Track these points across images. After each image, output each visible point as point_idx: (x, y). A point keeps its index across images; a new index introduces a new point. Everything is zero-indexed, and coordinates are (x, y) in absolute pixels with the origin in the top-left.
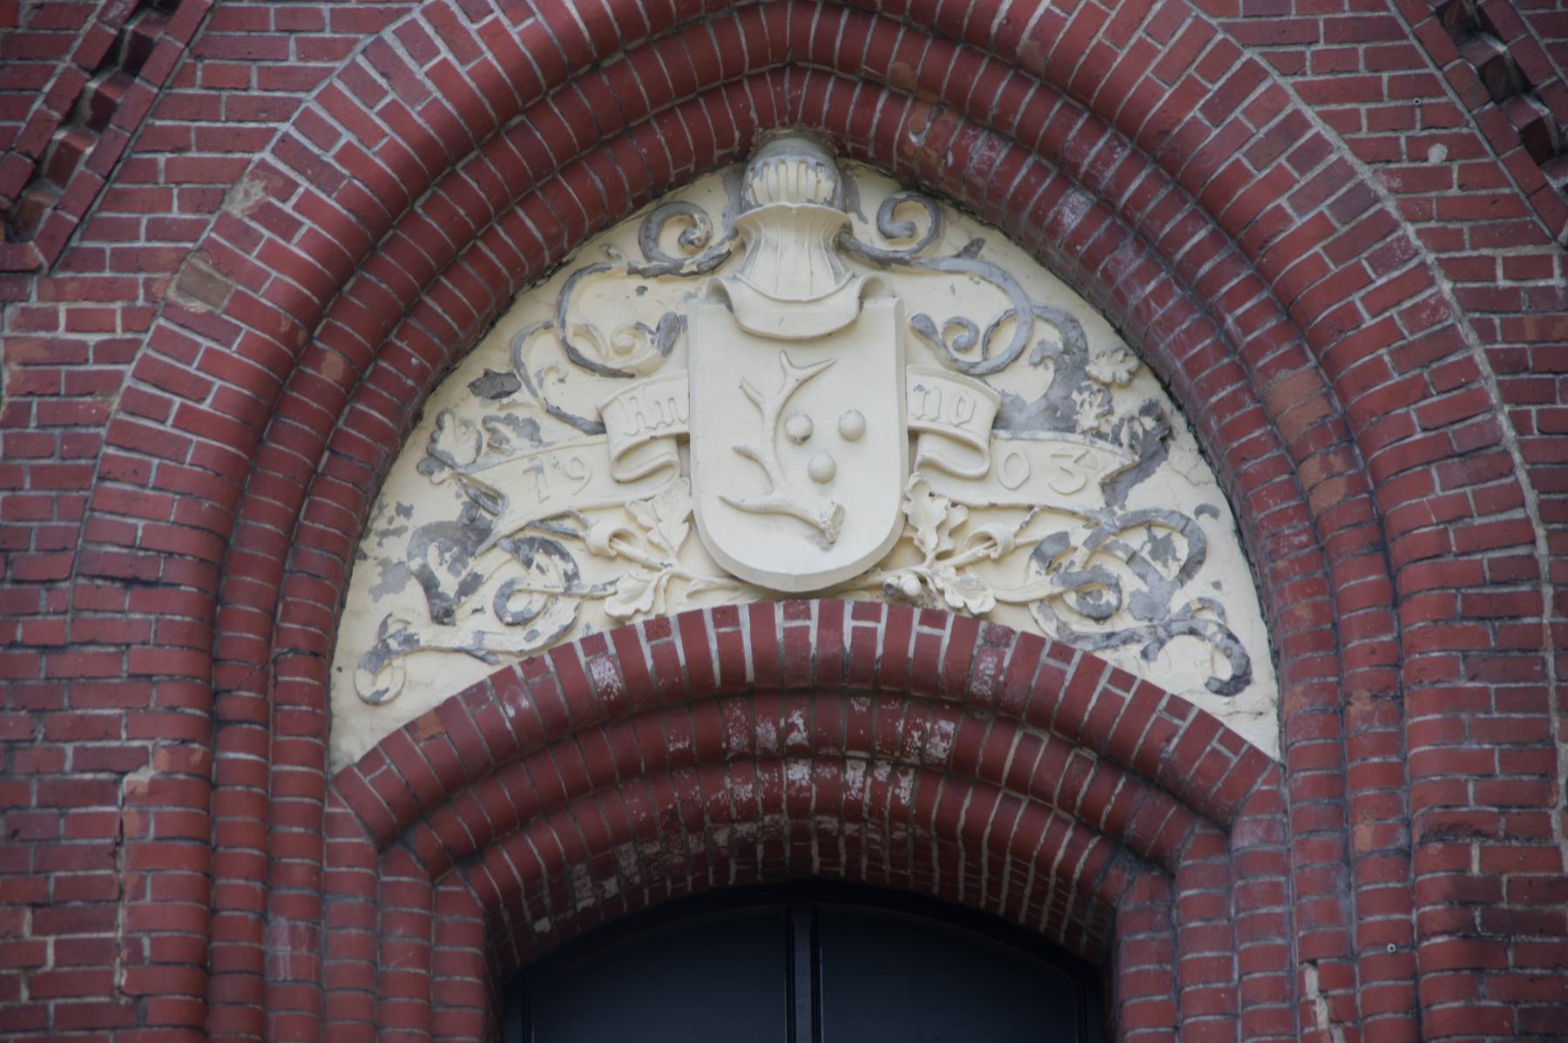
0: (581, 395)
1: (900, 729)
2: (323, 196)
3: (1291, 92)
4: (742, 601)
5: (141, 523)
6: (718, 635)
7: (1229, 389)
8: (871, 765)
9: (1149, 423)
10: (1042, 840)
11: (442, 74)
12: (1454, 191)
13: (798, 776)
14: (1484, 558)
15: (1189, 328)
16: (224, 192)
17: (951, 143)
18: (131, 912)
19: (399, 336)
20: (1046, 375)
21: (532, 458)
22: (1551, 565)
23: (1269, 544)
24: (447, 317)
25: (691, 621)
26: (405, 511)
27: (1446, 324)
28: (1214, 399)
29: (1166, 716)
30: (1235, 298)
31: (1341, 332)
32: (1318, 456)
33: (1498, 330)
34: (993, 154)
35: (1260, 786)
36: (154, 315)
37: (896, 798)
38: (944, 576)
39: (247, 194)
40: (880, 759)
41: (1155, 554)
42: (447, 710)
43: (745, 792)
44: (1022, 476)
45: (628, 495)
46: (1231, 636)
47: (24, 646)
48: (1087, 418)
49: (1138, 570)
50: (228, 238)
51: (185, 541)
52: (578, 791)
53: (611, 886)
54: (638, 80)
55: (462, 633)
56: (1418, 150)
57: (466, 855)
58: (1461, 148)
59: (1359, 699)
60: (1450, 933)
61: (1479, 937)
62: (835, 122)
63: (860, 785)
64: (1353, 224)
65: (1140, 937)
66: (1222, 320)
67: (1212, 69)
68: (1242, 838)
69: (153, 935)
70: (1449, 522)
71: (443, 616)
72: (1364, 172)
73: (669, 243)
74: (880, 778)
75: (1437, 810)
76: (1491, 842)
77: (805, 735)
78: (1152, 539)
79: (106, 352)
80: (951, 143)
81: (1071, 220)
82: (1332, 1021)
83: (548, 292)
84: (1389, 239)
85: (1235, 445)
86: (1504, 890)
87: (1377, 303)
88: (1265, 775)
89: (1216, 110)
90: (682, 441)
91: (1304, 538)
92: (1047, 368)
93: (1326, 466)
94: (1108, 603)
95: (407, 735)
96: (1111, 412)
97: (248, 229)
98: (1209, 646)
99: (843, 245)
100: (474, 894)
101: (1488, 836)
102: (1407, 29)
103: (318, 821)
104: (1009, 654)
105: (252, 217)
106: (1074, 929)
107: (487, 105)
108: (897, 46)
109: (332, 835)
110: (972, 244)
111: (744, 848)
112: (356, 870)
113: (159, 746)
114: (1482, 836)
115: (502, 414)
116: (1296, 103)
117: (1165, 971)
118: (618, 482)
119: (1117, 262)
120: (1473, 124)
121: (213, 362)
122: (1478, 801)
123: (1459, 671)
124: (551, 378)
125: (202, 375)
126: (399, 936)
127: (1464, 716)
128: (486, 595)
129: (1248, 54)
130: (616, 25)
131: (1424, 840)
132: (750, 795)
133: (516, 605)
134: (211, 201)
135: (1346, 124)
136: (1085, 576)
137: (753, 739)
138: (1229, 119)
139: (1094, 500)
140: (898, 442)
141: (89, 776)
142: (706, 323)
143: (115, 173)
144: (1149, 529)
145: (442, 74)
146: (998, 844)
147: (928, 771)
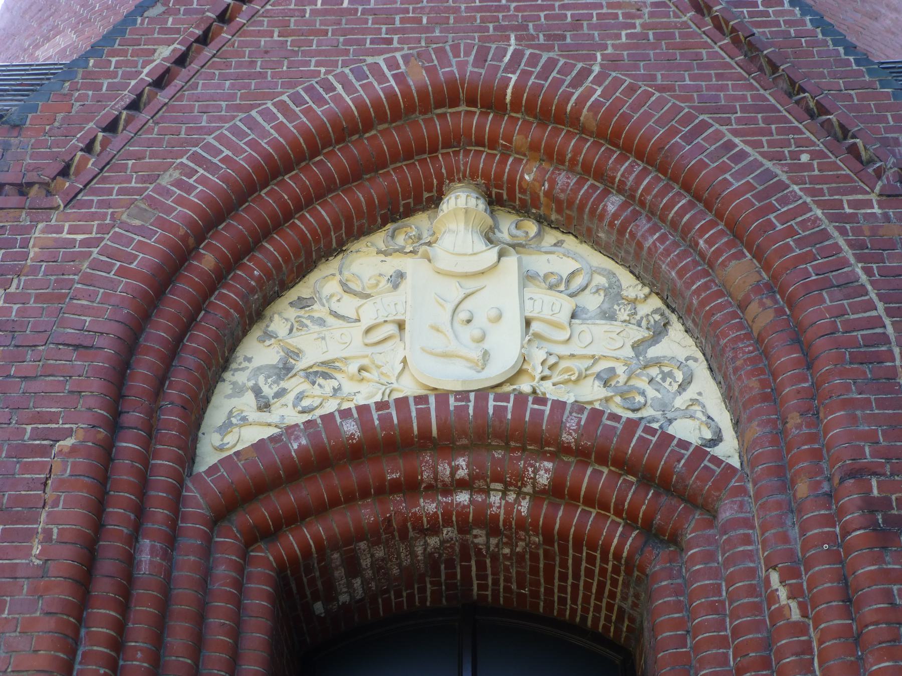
0: (348, 305)
1: (522, 466)
2: (210, 176)
3: (726, 132)
5: (88, 319)
6: (417, 409)
7: (703, 281)
8: (504, 494)
9: (657, 317)
10: (604, 534)
11: (280, 128)
12: (816, 172)
13: (462, 499)
15: (678, 253)
16: (159, 175)
17: (546, 178)
18: (49, 514)
19: (249, 260)
20: (599, 299)
21: (319, 333)
22: (896, 338)
23: (731, 354)
24: (275, 253)
25: (402, 403)
26: (249, 360)
27: (821, 228)
28: (694, 287)
29: (677, 449)
30: (703, 230)
31: (765, 232)
32: (757, 301)
33: (849, 231)
34: (569, 181)
35: (733, 483)
36: (113, 226)
37: (519, 512)
39: (171, 175)
40: (510, 491)
41: (664, 380)
44: (589, 340)
45: (369, 351)
46: (709, 417)
47: (14, 377)
48: (623, 315)
49: (656, 387)
50: (158, 194)
51: (114, 329)
52: (334, 502)
54: (383, 143)
55: (274, 416)
56: (795, 156)
58: (815, 155)
59: (792, 418)
60: (865, 528)
61: (882, 530)
62: (486, 175)
63: (498, 505)
64: (766, 185)
65: (664, 583)
66: (697, 244)
68: (725, 513)
69: (60, 527)
70: (837, 317)
71: (265, 406)
72: (768, 164)
73: (401, 240)
74: (510, 501)
75: (848, 462)
76: (883, 478)
77: (466, 471)
78: (662, 372)
79: (84, 243)
80: (546, 178)
81: (611, 208)
82: (789, 598)
84: (785, 192)
85: (708, 308)
86: (894, 504)
87: (783, 218)
88: (736, 478)
90: (401, 326)
91: (751, 348)
92: (599, 295)
93: (762, 304)
94: (639, 402)
95: (235, 458)
96: (635, 313)
97: (168, 190)
98: (698, 422)
99: (489, 238)
100: (271, 558)
101: (881, 475)
102: (782, 109)
104: (584, 417)
105: (172, 185)
107: (302, 141)
108: (518, 127)
109: (184, 507)
110: (558, 243)
112: (198, 526)
113: (80, 427)
114: (877, 475)
115: (307, 315)
116: (729, 136)
117: (680, 601)
118: (366, 345)
119: (637, 226)
120: (821, 145)
121: (141, 246)
122: (872, 456)
123: (852, 389)
124: (335, 299)
125: (134, 252)
127: (858, 413)
128: (290, 398)
129: (701, 117)
130: (371, 110)
131: (842, 480)
132: (435, 510)
133: (305, 403)
135: (756, 145)
136: (625, 388)
137: (436, 473)
138: (695, 142)
139: (629, 352)
140: (517, 325)
141: (38, 442)
143: (106, 169)
144: (660, 367)
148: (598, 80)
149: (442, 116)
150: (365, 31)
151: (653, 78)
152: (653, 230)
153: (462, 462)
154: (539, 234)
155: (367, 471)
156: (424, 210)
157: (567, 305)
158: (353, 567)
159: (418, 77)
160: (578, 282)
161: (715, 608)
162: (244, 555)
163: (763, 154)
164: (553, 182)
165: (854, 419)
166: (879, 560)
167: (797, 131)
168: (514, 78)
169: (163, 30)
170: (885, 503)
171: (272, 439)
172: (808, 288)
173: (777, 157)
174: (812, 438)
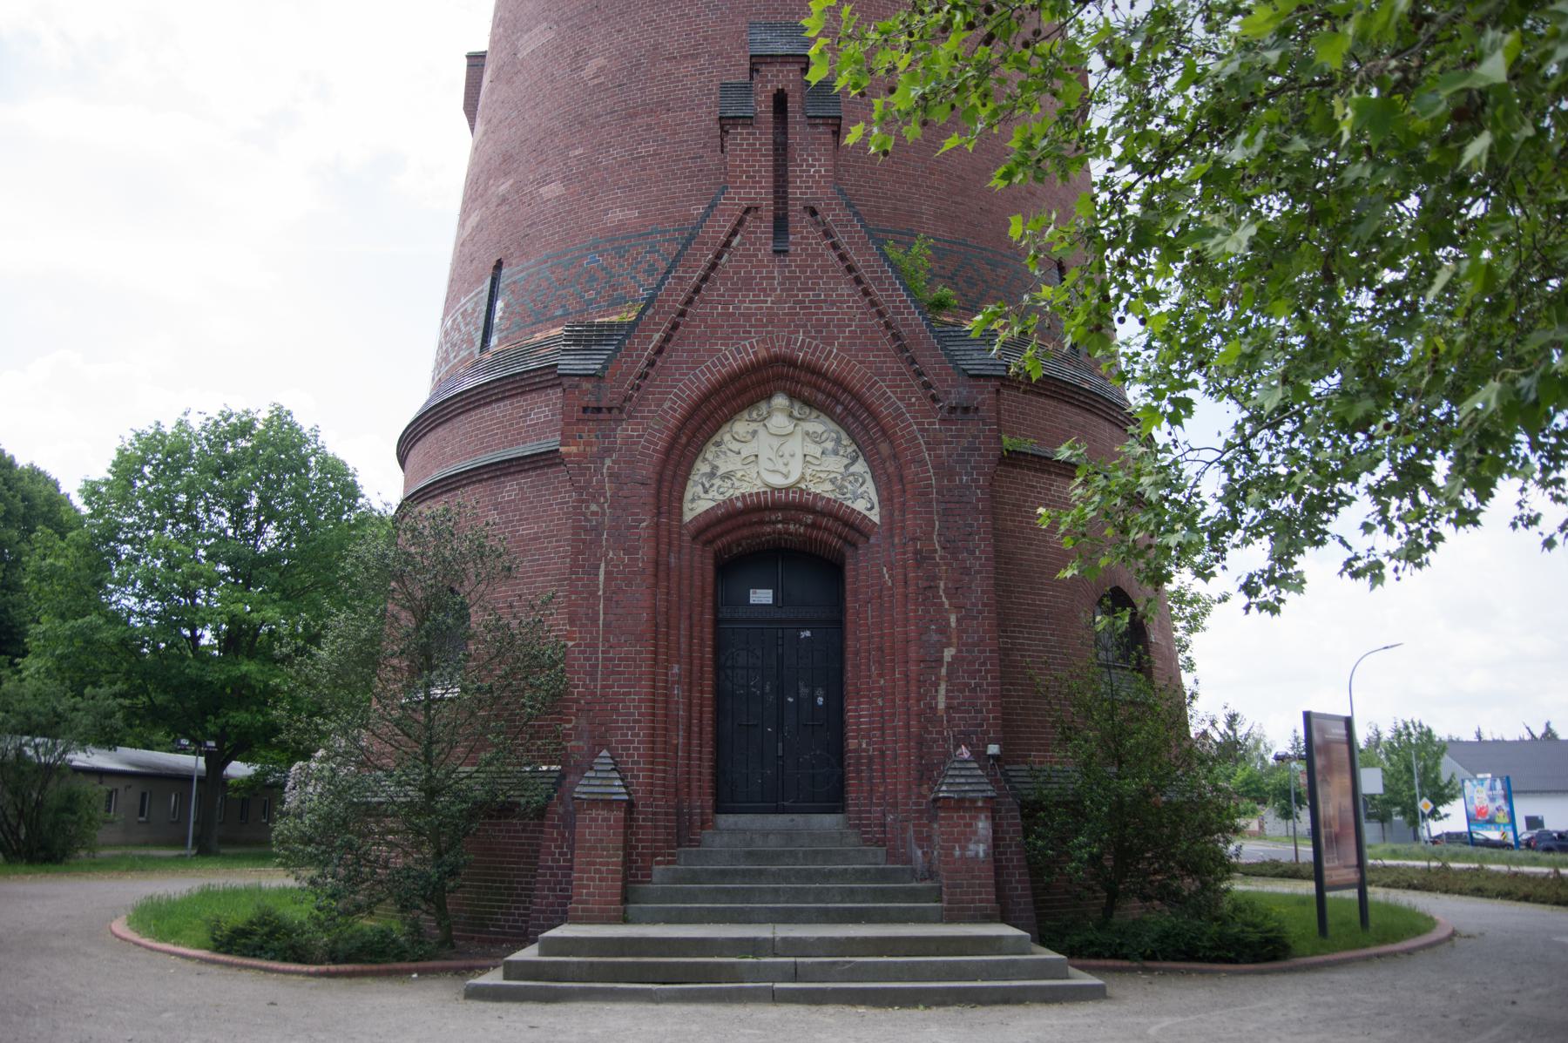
0: (735, 446)
11: (708, 379)
48: (841, 453)
55: (710, 496)
58: (918, 399)
67: (868, 381)
71: (706, 492)
79: (638, 436)
83: (729, 424)
87: (901, 430)
99: (791, 416)
103: (680, 534)
111: (768, 541)
121: (660, 439)
128: (715, 488)
139: (842, 470)
142: (762, 433)
145: (708, 379)
147: (807, 526)
148: (835, 358)
150: (740, 326)
158: (740, 545)
159: (763, 354)
169: (655, 324)
171: (712, 508)
173: (901, 399)
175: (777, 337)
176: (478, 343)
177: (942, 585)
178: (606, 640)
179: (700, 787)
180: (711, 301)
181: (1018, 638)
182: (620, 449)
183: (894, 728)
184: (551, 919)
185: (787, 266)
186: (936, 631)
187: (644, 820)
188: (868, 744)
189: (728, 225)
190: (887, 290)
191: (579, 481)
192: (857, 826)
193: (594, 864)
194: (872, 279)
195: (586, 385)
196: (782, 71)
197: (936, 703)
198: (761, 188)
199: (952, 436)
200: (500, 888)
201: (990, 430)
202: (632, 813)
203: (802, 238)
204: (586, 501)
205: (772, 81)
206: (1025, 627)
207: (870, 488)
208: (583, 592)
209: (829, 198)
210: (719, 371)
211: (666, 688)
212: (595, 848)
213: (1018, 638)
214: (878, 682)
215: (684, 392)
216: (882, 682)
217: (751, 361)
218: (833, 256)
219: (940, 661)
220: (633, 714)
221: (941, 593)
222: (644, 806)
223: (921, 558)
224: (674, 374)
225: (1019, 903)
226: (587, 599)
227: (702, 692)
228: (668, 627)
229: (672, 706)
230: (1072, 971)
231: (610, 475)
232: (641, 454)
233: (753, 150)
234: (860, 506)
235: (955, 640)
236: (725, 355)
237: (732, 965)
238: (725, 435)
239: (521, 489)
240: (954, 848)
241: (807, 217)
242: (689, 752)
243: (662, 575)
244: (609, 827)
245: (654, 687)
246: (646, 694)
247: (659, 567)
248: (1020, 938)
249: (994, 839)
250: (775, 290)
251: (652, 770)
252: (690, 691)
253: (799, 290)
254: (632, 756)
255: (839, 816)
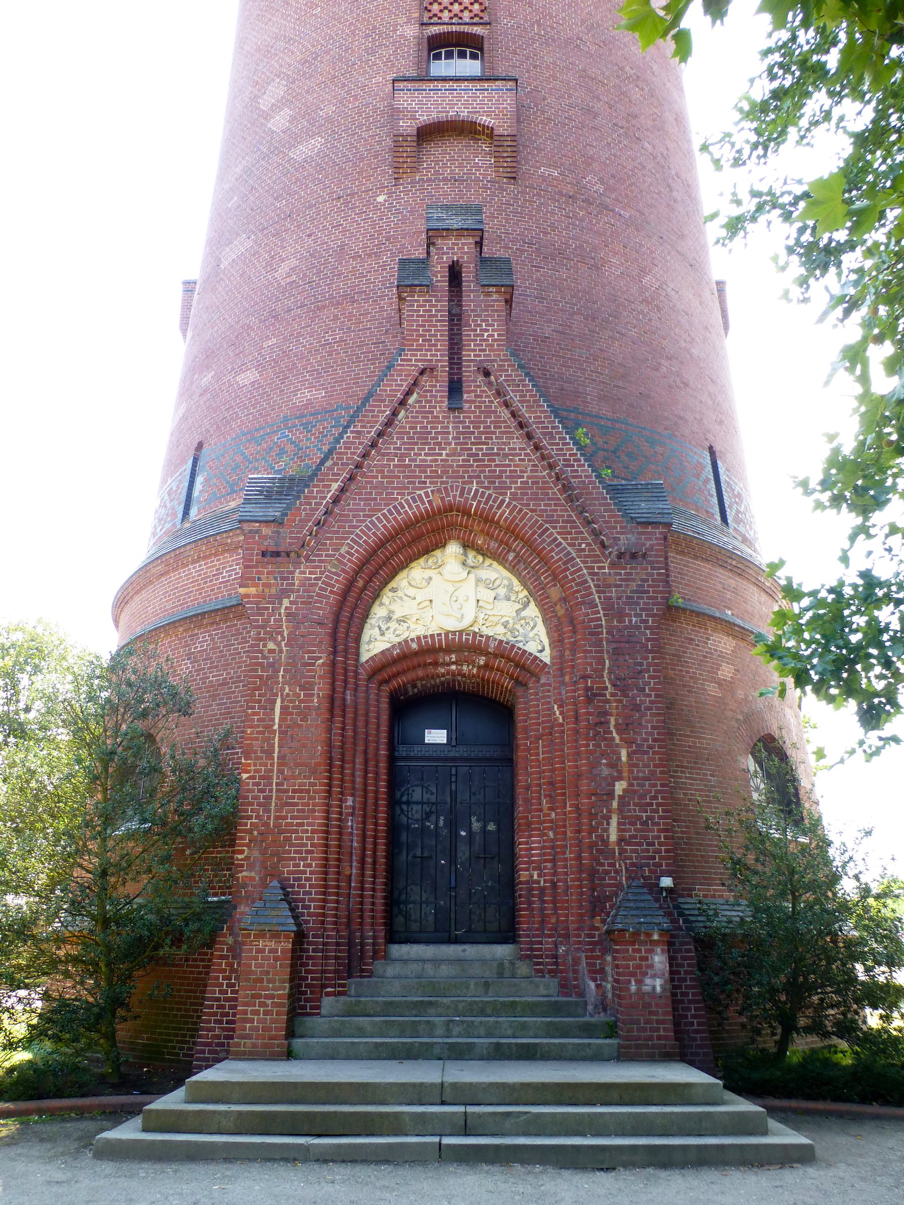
0: (411, 592)
4: (443, 632)
11: (384, 526)
14: (592, 624)
20: (505, 589)
25: (432, 636)
30: (543, 573)
38: (484, 629)
42: (383, 652)
43: (443, 671)
48: (513, 598)
52: (409, 669)
53: (416, 690)
55: (386, 638)
56: (580, 545)
57: (385, 681)
58: (588, 544)
67: (539, 528)
71: (383, 634)
72: (569, 549)
73: (430, 561)
79: (315, 579)
81: (511, 558)
83: (405, 572)
89: (540, 536)
90: (431, 601)
99: (464, 564)
103: (356, 672)
106: (508, 701)
111: (442, 683)
116: (556, 535)
121: (337, 581)
126: (372, 696)
128: (391, 630)
133: (397, 632)
134: (337, 550)
135: (565, 539)
142: (436, 578)
145: (384, 526)
146: (493, 682)
147: (479, 667)
148: (507, 507)
149: (447, 516)
151: (529, 505)
152: (525, 569)
153: (453, 656)
154: (483, 562)
155: (420, 659)
156: (439, 548)
157: (492, 594)
158: (414, 686)
159: (437, 502)
160: (496, 584)
161: (537, 712)
162: (379, 690)
163: (568, 544)
164: (489, 545)
165: (586, 658)
166: (587, 708)
167: (582, 533)
168: (475, 504)
169: (333, 474)
170: (592, 688)
172: (577, 604)
174: (572, 660)
175: (452, 487)
176: (180, 516)
177: (613, 722)
178: (280, 772)
179: (373, 917)
180: (388, 454)
181: (681, 778)
182: (298, 591)
183: (566, 860)
184: (216, 1052)
185: (461, 422)
186: (607, 765)
187: (314, 951)
188: (539, 875)
189: (405, 384)
190: (558, 444)
191: (257, 621)
192: (527, 956)
193: (259, 996)
194: (542, 433)
195: (266, 531)
196: (457, 244)
197: (608, 837)
198: (436, 350)
199: (621, 580)
200: (176, 1016)
201: (659, 574)
202: (302, 944)
203: (476, 396)
204: (264, 639)
205: (448, 253)
206: (687, 768)
207: (541, 630)
208: (258, 726)
209: (502, 360)
210: (395, 518)
211: (339, 820)
212: (261, 981)
213: (681, 778)
214: (549, 815)
215: (361, 538)
216: (553, 815)
217: (426, 509)
218: (505, 414)
219: (611, 794)
220: (305, 845)
221: (612, 729)
222: (314, 936)
223: (591, 696)
224: (352, 521)
225: (695, 1039)
226: (263, 733)
227: (376, 824)
228: (342, 760)
229: (345, 837)
230: (772, 1124)
231: (288, 615)
232: (318, 595)
233: (429, 316)
234: (532, 648)
235: (625, 774)
236: (400, 504)
237: (396, 1115)
238: (402, 581)
239: (213, 640)
240: (629, 982)
241: (481, 378)
242: (362, 882)
243: (337, 711)
244: (276, 959)
245: (327, 818)
246: (319, 825)
247: (334, 704)
248: (717, 1084)
249: (671, 972)
250: (450, 444)
251: (324, 901)
252: (364, 823)
253: (472, 444)
254: (304, 886)
255: (511, 946)
